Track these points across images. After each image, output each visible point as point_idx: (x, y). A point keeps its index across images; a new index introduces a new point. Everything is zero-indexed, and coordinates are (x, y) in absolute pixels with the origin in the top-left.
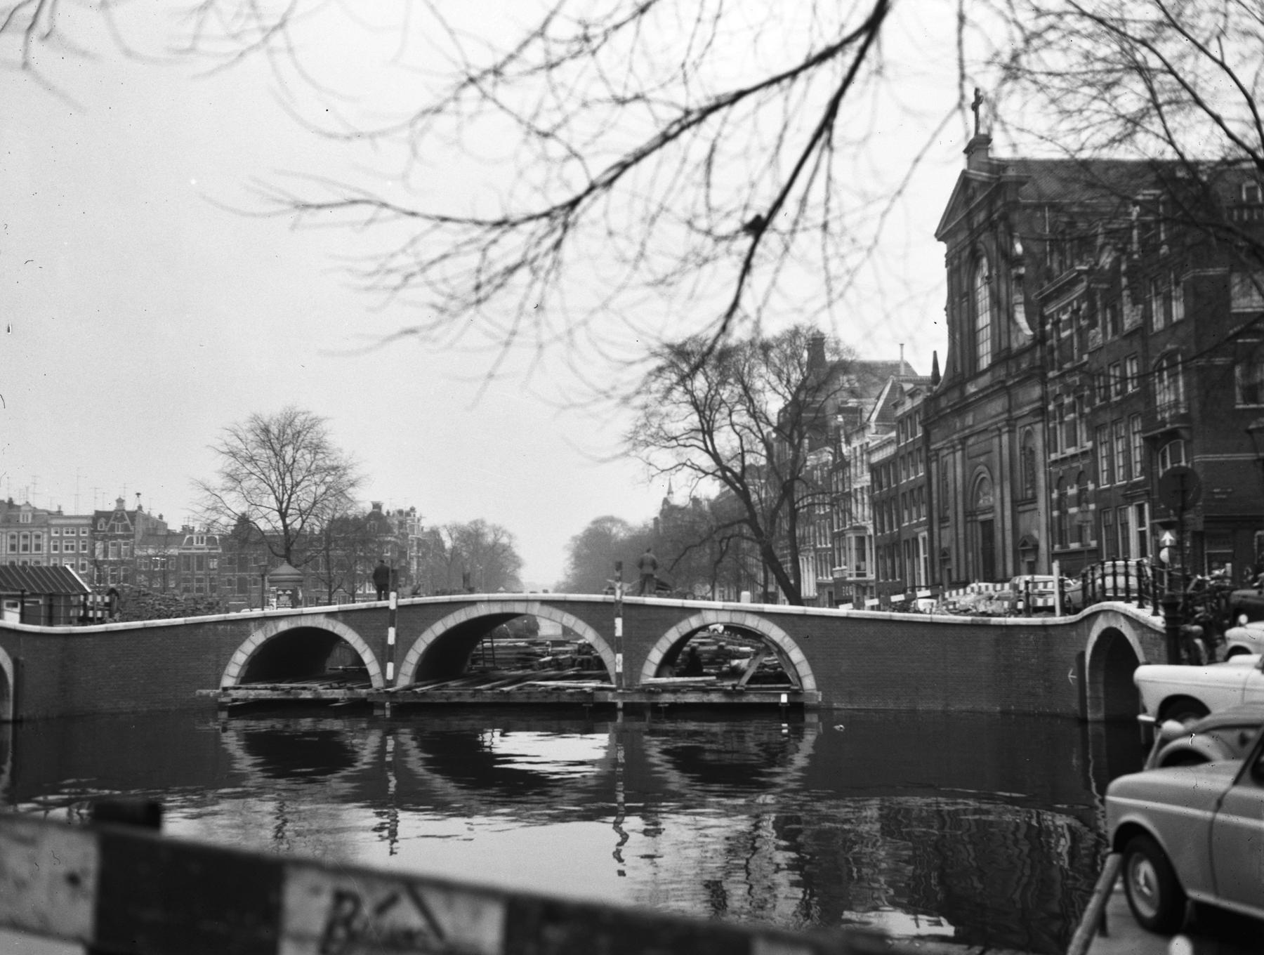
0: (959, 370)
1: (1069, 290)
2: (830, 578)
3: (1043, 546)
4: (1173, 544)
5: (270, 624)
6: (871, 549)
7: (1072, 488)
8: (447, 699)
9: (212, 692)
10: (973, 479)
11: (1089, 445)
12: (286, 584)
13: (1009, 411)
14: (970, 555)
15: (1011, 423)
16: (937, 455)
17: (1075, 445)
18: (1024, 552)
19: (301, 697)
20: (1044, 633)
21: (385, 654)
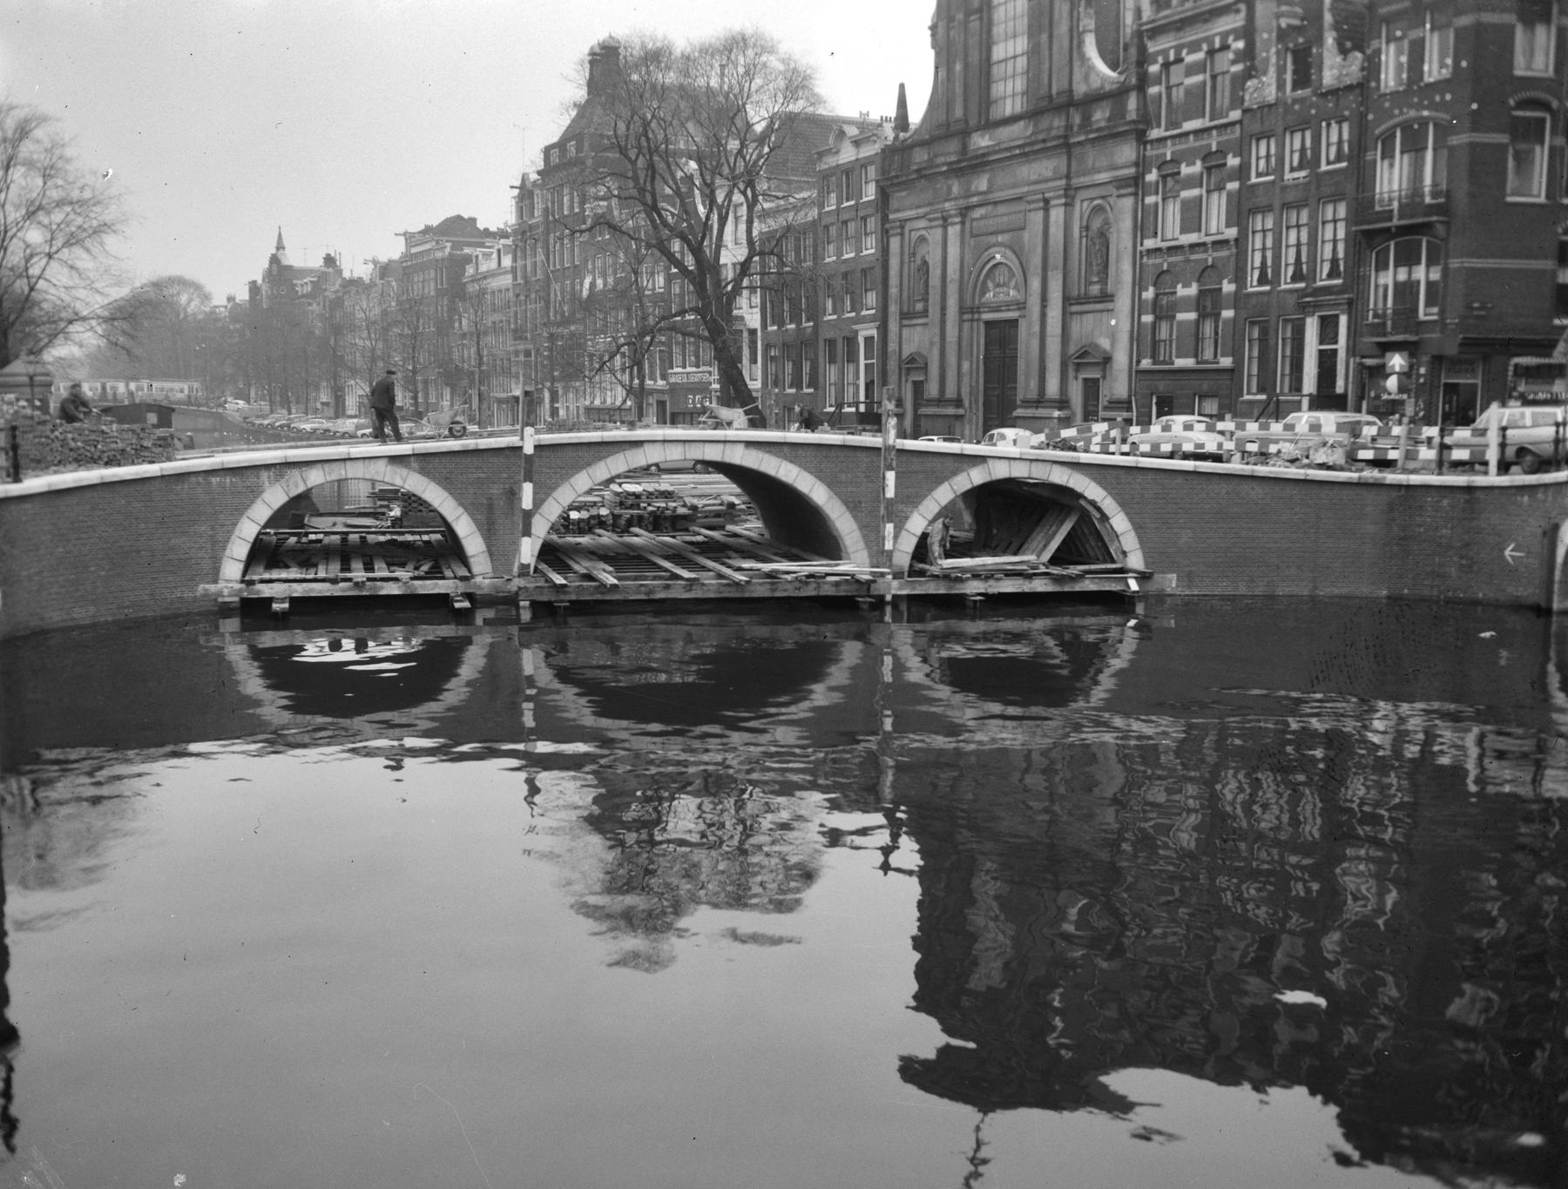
0: (959, 112)
1: (1206, 21)
2: (661, 383)
3: (1121, 359)
4: (1406, 369)
5: (295, 472)
8: (648, 594)
9: (212, 588)
10: (978, 265)
11: (1232, 233)
13: (1068, 177)
14: (966, 366)
15: (1070, 194)
16: (902, 227)
18: (1078, 367)
20: (1468, 497)
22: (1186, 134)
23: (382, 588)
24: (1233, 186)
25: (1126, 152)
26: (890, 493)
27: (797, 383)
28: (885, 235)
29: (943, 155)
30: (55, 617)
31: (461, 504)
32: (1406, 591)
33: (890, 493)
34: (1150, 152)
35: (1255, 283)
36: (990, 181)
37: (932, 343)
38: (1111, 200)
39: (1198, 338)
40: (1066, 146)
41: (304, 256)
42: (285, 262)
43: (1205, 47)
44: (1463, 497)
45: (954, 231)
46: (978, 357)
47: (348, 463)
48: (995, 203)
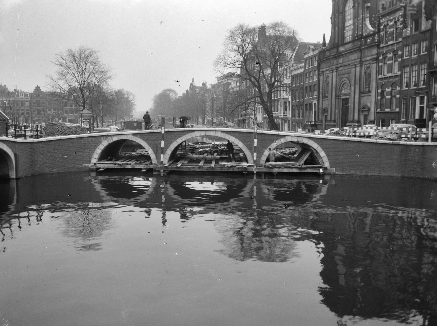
0: (336, 41)
1: (394, 13)
3: (372, 109)
5: (110, 138)
6: (289, 106)
7: (388, 88)
8: (189, 169)
10: (340, 83)
11: (399, 73)
12: (87, 117)
13: (361, 58)
14: (337, 111)
15: (361, 63)
16: (323, 73)
17: (392, 72)
18: (363, 111)
19: (127, 167)
20: (423, 148)
21: (159, 151)
22: (389, 45)
23: (126, 166)
24: (400, 60)
25: (375, 51)
26: (255, 145)
27: (299, 116)
28: (319, 75)
29: (333, 53)
30: (47, 171)
31: (150, 146)
32: (406, 175)
33: (255, 145)
34: (381, 51)
35: (405, 87)
36: (343, 60)
37: (329, 105)
38: (371, 64)
39: (391, 103)
40: (360, 50)
41: (198, 84)
42: (194, 85)
43: (394, 20)
44: (422, 148)
45: (334, 74)
46: (340, 108)
47: (123, 135)
48: (344, 66)
